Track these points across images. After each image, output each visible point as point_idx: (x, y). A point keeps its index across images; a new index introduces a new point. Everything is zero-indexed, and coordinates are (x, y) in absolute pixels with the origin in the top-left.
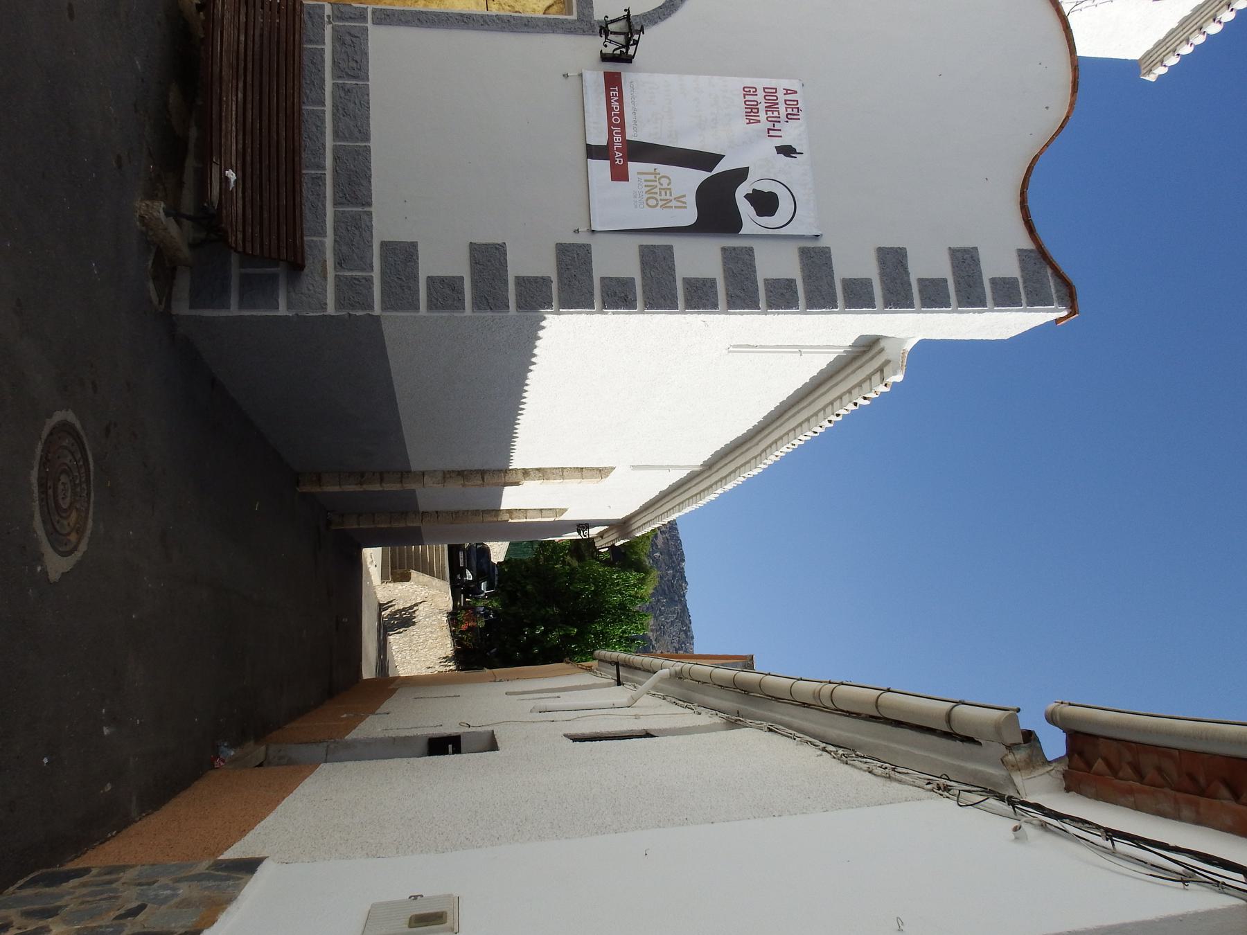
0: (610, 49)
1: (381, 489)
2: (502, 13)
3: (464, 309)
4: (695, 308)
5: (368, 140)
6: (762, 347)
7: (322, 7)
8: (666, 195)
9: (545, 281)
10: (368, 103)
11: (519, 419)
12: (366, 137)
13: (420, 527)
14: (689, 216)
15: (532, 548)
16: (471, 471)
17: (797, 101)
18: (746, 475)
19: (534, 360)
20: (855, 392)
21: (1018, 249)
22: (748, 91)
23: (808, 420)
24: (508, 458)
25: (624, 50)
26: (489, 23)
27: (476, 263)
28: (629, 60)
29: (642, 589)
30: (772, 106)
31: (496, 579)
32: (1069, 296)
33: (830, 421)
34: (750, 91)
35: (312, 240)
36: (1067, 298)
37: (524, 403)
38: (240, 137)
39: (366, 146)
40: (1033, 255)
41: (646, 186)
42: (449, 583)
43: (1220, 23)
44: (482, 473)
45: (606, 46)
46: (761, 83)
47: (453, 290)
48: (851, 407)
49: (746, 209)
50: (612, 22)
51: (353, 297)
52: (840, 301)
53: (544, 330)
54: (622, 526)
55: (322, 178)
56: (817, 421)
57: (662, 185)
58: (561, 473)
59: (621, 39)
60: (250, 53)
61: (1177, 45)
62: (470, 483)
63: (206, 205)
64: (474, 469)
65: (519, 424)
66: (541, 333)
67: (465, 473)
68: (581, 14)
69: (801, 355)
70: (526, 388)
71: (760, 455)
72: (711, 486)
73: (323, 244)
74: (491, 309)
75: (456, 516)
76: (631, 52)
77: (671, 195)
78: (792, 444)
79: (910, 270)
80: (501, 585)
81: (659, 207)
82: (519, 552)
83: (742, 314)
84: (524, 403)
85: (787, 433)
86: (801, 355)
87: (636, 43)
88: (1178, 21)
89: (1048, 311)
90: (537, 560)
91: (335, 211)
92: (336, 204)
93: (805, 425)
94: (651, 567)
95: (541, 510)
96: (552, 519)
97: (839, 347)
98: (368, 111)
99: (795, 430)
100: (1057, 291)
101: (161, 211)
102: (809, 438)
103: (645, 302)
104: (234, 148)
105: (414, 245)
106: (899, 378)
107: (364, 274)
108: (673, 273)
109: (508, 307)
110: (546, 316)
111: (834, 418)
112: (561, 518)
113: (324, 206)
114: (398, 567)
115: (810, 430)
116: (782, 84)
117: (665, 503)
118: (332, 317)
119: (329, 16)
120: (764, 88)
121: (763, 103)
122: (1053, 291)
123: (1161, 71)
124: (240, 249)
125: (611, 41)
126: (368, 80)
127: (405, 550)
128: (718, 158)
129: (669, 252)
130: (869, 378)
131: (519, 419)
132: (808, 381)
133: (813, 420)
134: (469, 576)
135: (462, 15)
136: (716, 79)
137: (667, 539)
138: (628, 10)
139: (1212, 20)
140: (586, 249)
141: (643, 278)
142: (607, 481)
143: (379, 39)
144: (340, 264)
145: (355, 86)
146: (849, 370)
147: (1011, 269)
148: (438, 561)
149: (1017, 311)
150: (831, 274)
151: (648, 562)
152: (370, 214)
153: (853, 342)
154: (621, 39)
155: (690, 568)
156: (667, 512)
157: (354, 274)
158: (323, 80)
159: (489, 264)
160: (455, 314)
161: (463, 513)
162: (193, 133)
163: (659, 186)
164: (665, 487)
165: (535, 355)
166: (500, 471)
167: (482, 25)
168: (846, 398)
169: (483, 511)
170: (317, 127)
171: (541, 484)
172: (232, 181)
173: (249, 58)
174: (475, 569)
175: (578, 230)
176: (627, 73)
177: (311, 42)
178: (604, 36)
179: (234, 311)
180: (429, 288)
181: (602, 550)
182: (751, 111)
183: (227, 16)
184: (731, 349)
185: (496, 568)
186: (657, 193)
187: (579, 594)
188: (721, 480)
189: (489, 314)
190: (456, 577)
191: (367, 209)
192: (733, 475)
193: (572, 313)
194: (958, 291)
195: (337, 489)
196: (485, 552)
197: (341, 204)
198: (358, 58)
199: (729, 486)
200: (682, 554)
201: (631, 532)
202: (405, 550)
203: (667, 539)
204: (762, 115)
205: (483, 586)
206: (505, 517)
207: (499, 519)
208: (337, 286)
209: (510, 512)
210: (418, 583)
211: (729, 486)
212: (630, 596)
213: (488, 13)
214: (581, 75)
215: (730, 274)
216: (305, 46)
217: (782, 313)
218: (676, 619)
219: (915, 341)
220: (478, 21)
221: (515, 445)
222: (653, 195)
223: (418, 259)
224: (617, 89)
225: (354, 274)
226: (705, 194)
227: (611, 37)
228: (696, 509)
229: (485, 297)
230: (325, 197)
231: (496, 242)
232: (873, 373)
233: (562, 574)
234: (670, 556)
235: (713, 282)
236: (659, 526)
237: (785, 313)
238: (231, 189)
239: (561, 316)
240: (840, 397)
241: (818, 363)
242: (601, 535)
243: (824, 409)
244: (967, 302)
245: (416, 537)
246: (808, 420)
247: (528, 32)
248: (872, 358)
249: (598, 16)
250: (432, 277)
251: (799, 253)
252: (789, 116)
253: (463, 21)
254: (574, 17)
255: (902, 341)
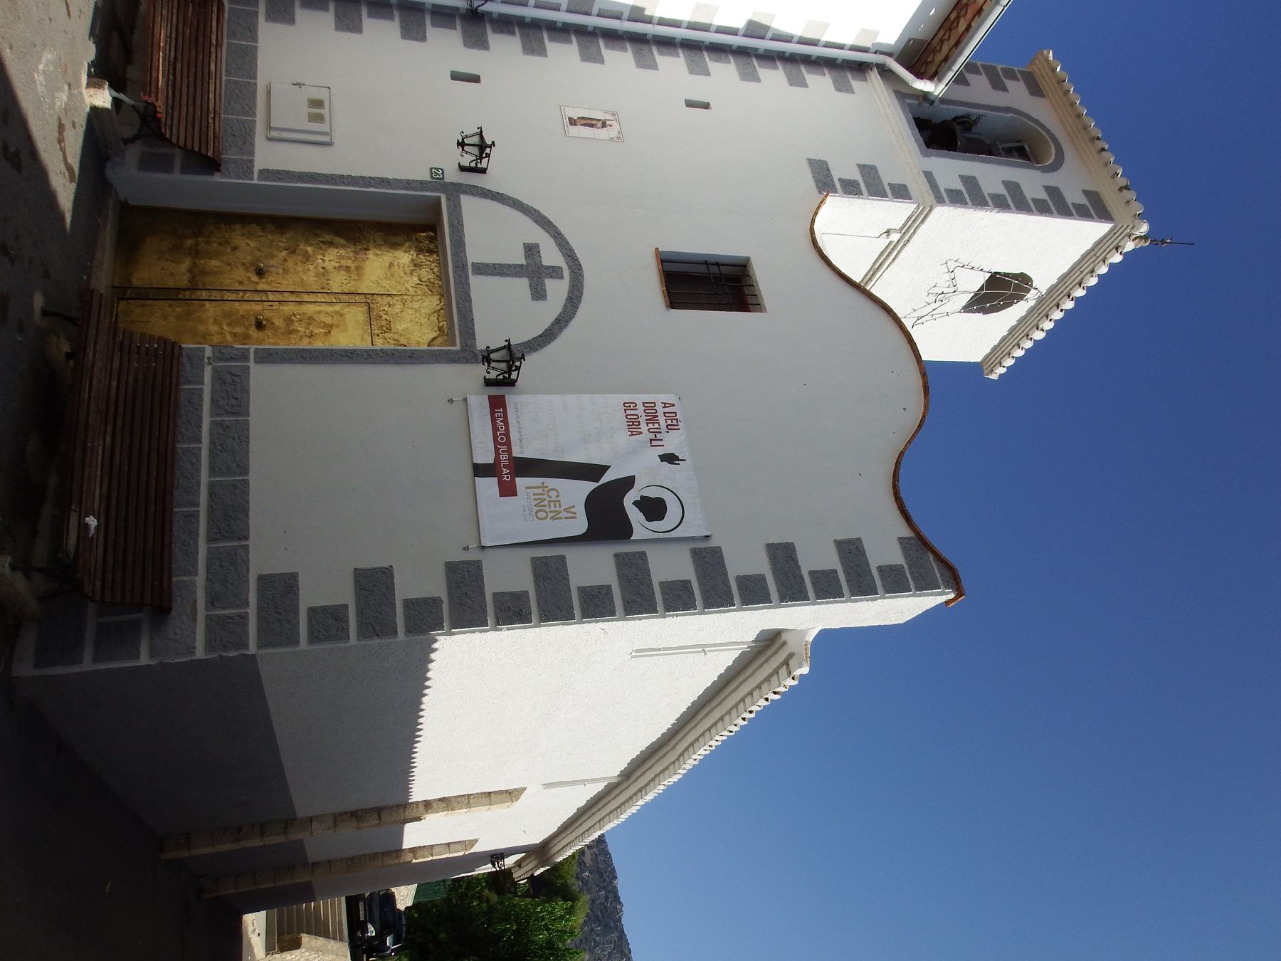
0: (493, 375)
1: (262, 844)
2: (387, 347)
3: (349, 638)
4: (592, 617)
5: (246, 473)
6: (664, 649)
7: (203, 350)
8: (555, 507)
9: (436, 601)
10: (248, 438)
11: (416, 748)
12: (245, 471)
13: (311, 881)
14: (580, 525)
15: (444, 885)
16: (366, 809)
17: (675, 413)
18: (666, 783)
19: (427, 683)
20: (765, 687)
21: (898, 538)
22: (628, 406)
23: (722, 719)
24: (406, 791)
25: (507, 376)
26: (373, 356)
27: (361, 589)
28: (512, 383)
29: (570, 921)
30: (652, 418)
31: (404, 929)
32: (953, 579)
33: (744, 719)
34: (630, 406)
35: (182, 580)
36: (952, 581)
37: (420, 730)
38: (106, 481)
39: (244, 480)
40: (913, 542)
41: (535, 499)
42: (347, 944)
43: (1043, 330)
44: (379, 811)
45: (489, 373)
46: (640, 399)
47: (337, 619)
48: (763, 703)
49: (635, 515)
50: (494, 351)
51: (226, 637)
52: (737, 599)
53: (437, 652)
54: (540, 851)
55: (195, 515)
56: (731, 720)
57: (550, 497)
58: (467, 801)
59: (503, 366)
60: (121, 398)
61: (1011, 349)
62: (365, 825)
63: (60, 555)
64: (368, 807)
65: (417, 752)
66: (433, 656)
67: (360, 813)
68: (464, 344)
69: (705, 654)
70: (421, 713)
71: (678, 759)
72: (631, 798)
73: (193, 583)
74: (378, 635)
75: (352, 863)
76: (514, 375)
77: (560, 507)
78: (709, 746)
79: (800, 563)
80: (410, 936)
81: (549, 518)
82: (430, 892)
83: (640, 619)
84: (420, 730)
85: (703, 734)
86: (705, 654)
87: (518, 368)
88: (1018, 319)
89: (936, 595)
90: (448, 900)
91: (209, 548)
92: (210, 539)
93: (720, 725)
94: (581, 890)
95: (449, 844)
96: (461, 854)
97: (742, 643)
98: (248, 445)
99: (710, 731)
100: (942, 575)
101: (7, 565)
102: (725, 738)
103: (541, 614)
104: (97, 492)
105: (294, 576)
106: (805, 670)
107: (238, 611)
108: (567, 583)
109: (396, 632)
110: (437, 637)
111: (748, 716)
112: (473, 850)
113: (197, 544)
114: (286, 932)
115: (725, 730)
116: (659, 399)
117: (585, 821)
118: (200, 661)
119: (209, 358)
120: (643, 403)
121: (643, 416)
122: (938, 575)
123: (1001, 371)
124: (98, 598)
125: (493, 369)
126: (248, 415)
127: (295, 910)
128: (604, 469)
129: (561, 562)
130: (776, 672)
131: (416, 748)
132: (716, 679)
133: (727, 718)
134: (372, 931)
135: (346, 351)
136: (597, 397)
137: (596, 855)
138: (508, 341)
139: (1035, 328)
140: (477, 565)
141: (537, 591)
142: (518, 804)
143: (261, 378)
144: (212, 603)
145: (234, 422)
146: (755, 665)
147: (896, 557)
148: (334, 919)
149: (907, 596)
150: (725, 573)
151: (575, 885)
152: (246, 548)
153: (755, 637)
154: (503, 366)
155: (624, 886)
156: (587, 830)
157: (227, 612)
158: (201, 418)
159: (375, 588)
160: (339, 645)
161: (360, 859)
162: (53, 480)
163: (548, 499)
164: (582, 803)
165: (428, 679)
166: (398, 806)
167: (366, 359)
168: (756, 694)
169: (383, 854)
170: (192, 464)
171: (445, 816)
172: (93, 527)
173: (121, 403)
174: (378, 922)
175: (468, 547)
176: (511, 396)
177: (189, 382)
178: (486, 364)
179: (87, 664)
180: (310, 620)
181: (521, 882)
182: (633, 424)
183: (99, 364)
184: (633, 654)
185: (403, 917)
186: (545, 506)
187: (499, 937)
188: (640, 790)
189: (376, 641)
190: (356, 934)
191: (243, 543)
192: (652, 784)
193: (464, 633)
194: (848, 581)
195: (209, 850)
196: (390, 898)
197: (216, 540)
198: (238, 396)
199: (650, 797)
200: (613, 871)
201: (549, 859)
202: (295, 910)
203: (596, 855)
204: (644, 428)
205: (389, 940)
206: (408, 857)
207: (401, 861)
208: (208, 627)
209: (413, 850)
210: (310, 949)
211: (650, 797)
212: (558, 931)
213: (373, 348)
214: (465, 400)
215: (624, 579)
216: (182, 387)
217: (680, 615)
218: (614, 949)
219: (816, 632)
220: (363, 355)
221: (413, 776)
222: (542, 508)
223: (298, 590)
224: (501, 410)
225: (227, 612)
226: (592, 503)
227: (493, 364)
228: (630, 816)
229: (371, 624)
230: (198, 535)
231: (383, 566)
232: (779, 667)
233: (479, 914)
234: (601, 875)
235: (608, 588)
236: (580, 847)
237: (684, 615)
238: (91, 535)
239: (454, 636)
240: (751, 693)
241: (724, 661)
242: (519, 864)
243: (736, 706)
244: (860, 591)
245: (307, 893)
246: (722, 719)
247: (412, 363)
248: (776, 652)
249: (481, 345)
250: (314, 607)
251: (691, 554)
252: (669, 427)
253: (347, 356)
254: (458, 348)
255: (804, 633)
